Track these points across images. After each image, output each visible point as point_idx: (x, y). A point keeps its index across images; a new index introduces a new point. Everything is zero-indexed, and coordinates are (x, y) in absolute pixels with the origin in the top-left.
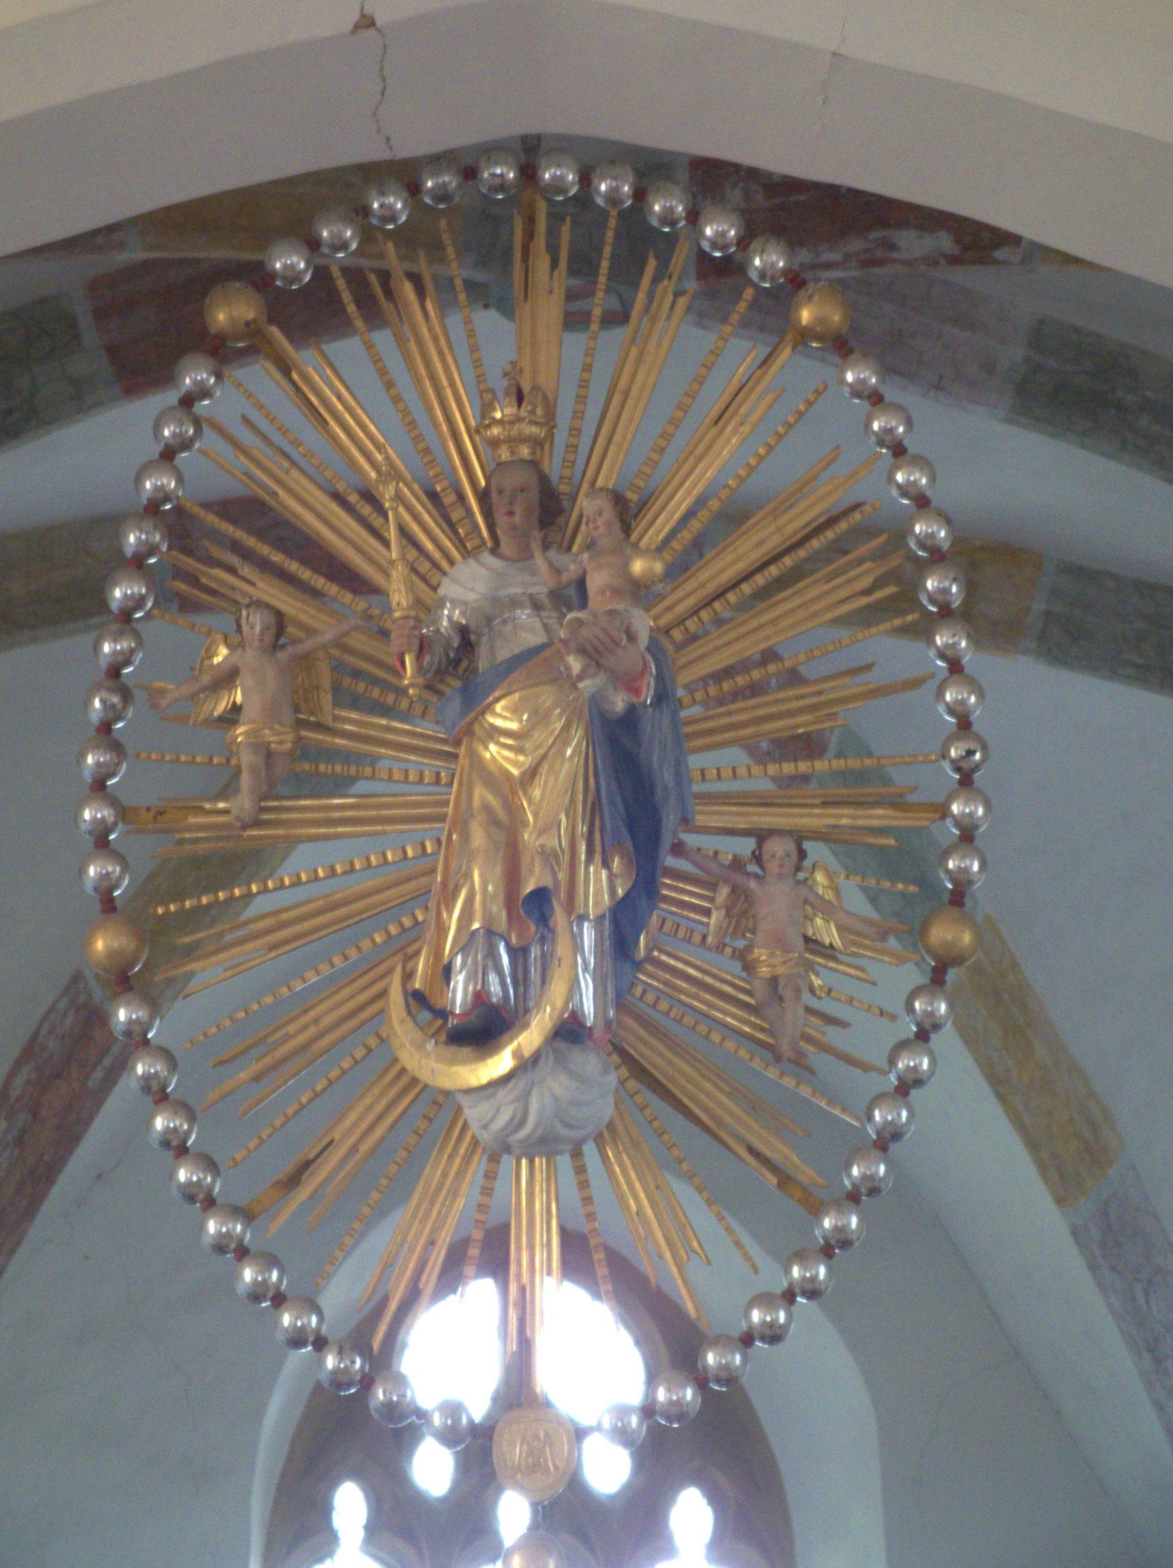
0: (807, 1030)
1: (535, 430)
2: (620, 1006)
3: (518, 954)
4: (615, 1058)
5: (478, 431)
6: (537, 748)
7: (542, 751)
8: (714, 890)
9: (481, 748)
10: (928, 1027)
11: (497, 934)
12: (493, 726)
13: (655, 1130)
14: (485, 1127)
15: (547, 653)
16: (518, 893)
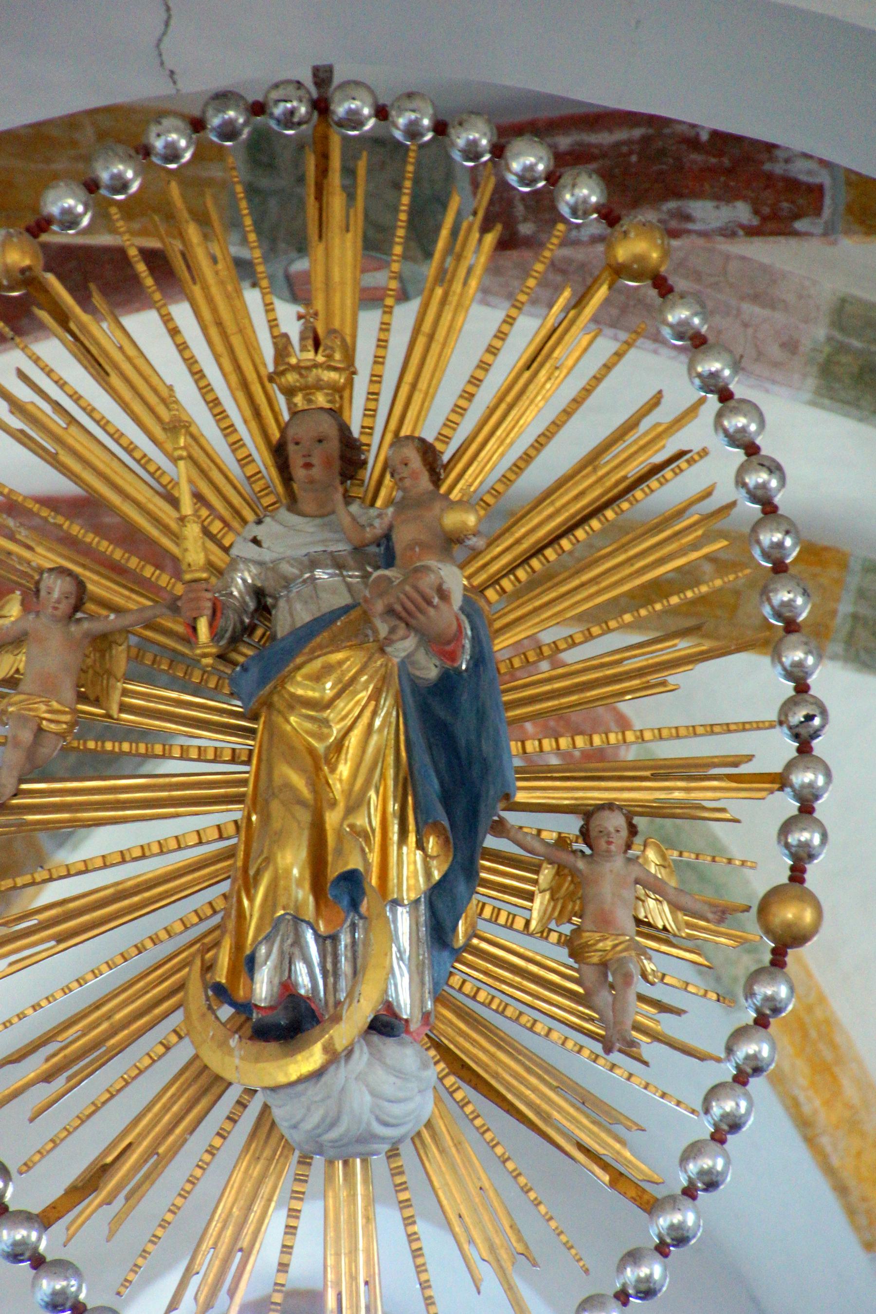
0: (639, 1018)
1: (334, 375)
2: (439, 998)
3: (328, 941)
4: (432, 1052)
5: (271, 379)
6: (343, 719)
7: (348, 722)
8: (537, 872)
9: (280, 720)
10: (768, 1012)
11: (303, 921)
12: (293, 695)
13: (477, 1129)
14: (295, 1127)
15: (354, 614)
16: (325, 876)
